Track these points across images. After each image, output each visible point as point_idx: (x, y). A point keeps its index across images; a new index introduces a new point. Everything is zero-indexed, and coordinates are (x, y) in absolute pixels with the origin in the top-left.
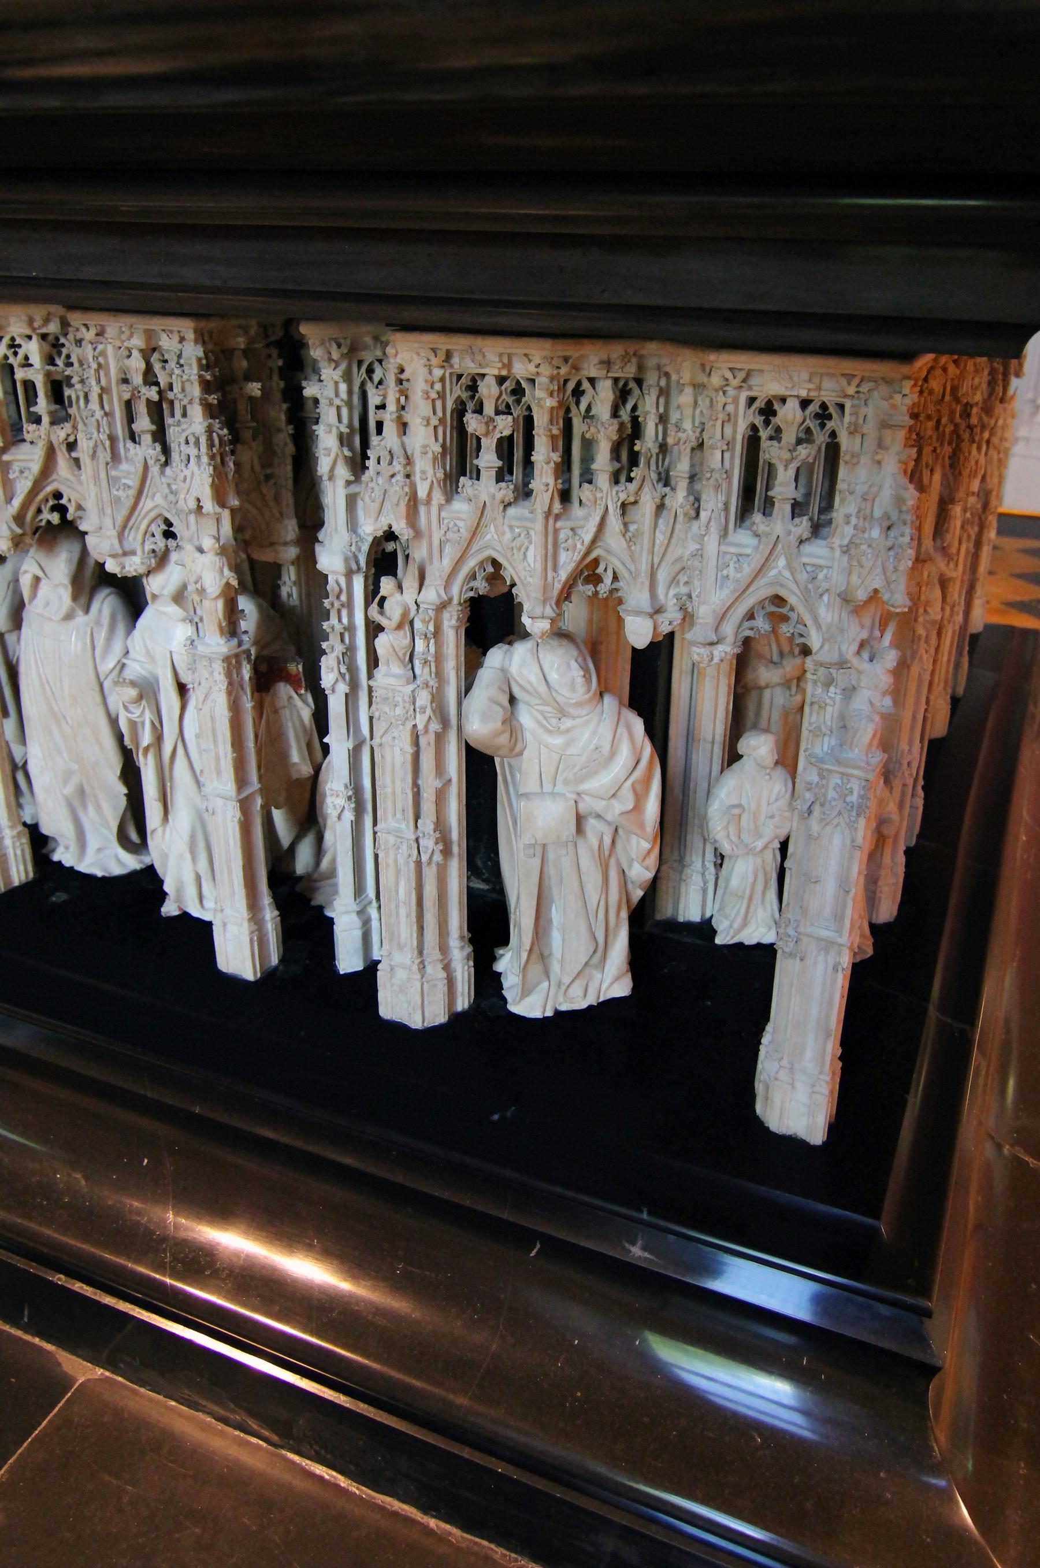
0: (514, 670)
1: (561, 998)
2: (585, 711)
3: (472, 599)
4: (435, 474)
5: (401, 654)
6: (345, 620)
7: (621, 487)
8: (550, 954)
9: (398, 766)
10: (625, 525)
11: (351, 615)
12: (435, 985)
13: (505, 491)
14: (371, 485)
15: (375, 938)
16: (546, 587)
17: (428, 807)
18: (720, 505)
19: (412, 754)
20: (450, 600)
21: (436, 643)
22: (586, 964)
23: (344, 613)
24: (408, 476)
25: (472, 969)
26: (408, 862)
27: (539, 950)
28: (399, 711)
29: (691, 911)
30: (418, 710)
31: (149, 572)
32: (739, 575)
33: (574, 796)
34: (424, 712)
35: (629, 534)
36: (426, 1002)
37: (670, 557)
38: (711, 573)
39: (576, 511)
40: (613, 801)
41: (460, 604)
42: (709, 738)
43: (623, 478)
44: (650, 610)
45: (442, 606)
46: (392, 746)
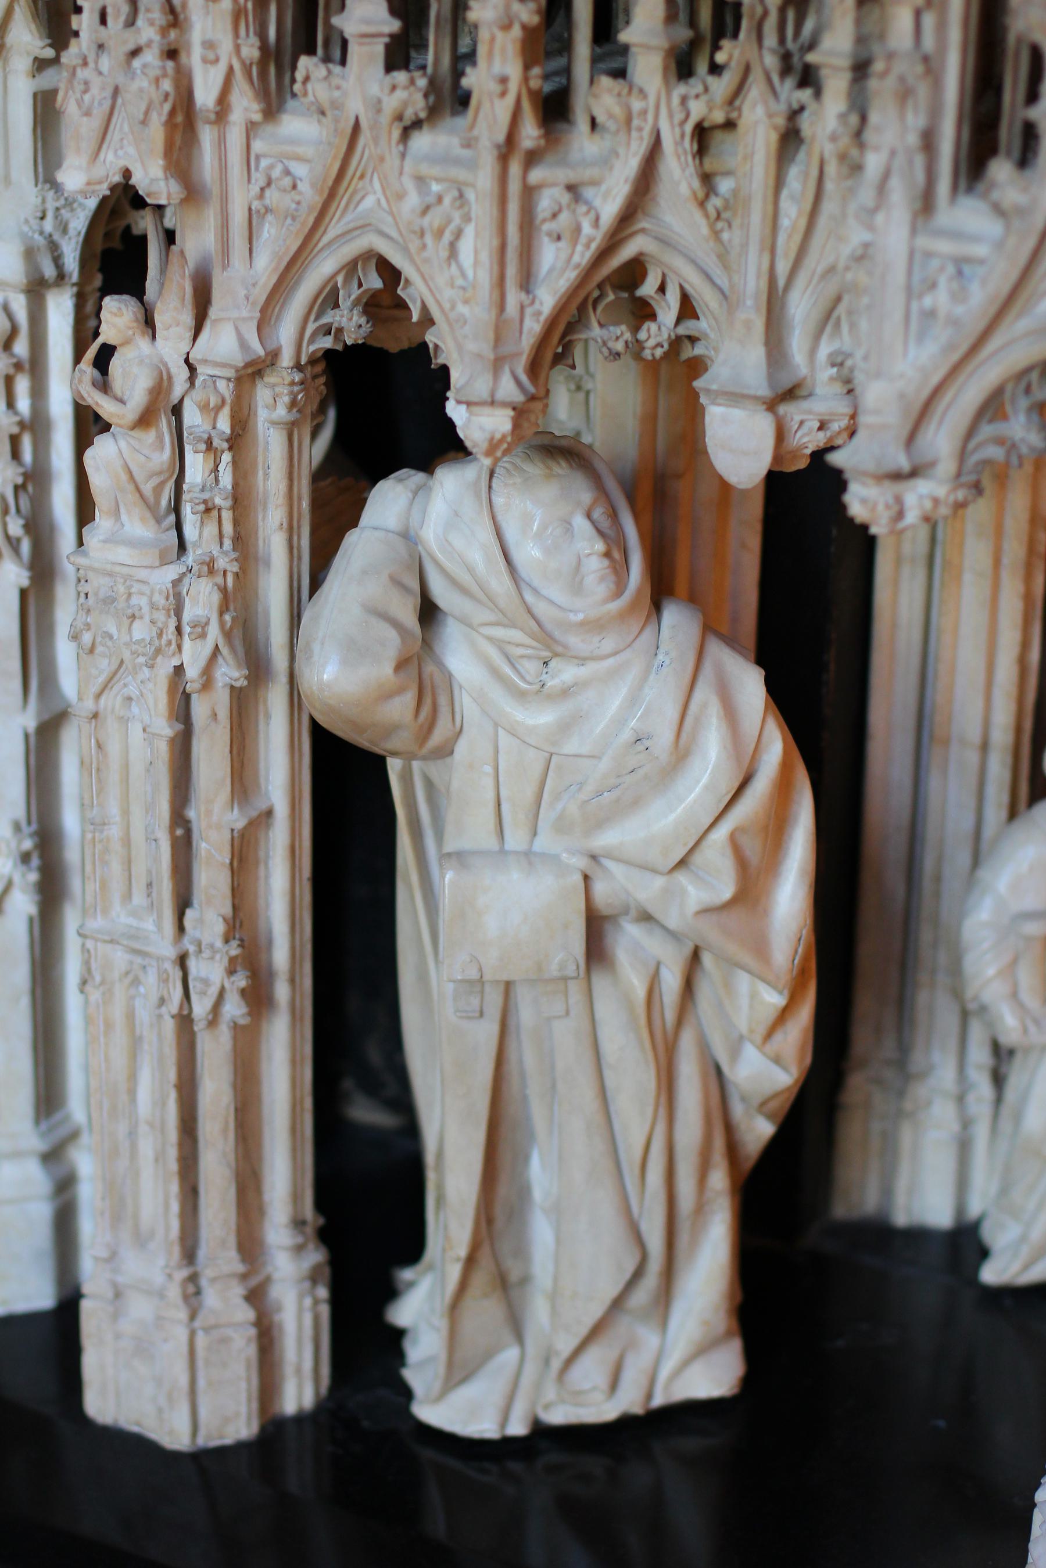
0: (431, 534)
1: (550, 1393)
2: (609, 644)
3: (329, 354)
4: (237, 48)
5: (147, 489)
6: (24, 404)
7: (694, 86)
8: (525, 1280)
9: (137, 769)
10: (707, 179)
11: (39, 392)
12: (225, 1341)
13: (407, 92)
14: (81, 74)
15: (89, 1228)
16: (499, 334)
17: (211, 878)
18: (913, 139)
19: (172, 741)
20: (274, 356)
21: (235, 463)
22: (617, 1304)
23: (22, 385)
24: (172, 54)
25: (325, 1310)
26: (160, 1016)
27: (496, 1257)
28: (140, 631)
29: (926, 1199)
30: (187, 630)
31: (456, 514)
32: (959, 310)
33: (580, 862)
34: (203, 636)
35: (715, 202)
36: (201, 1383)
37: (815, 262)
38: (895, 301)
39: (582, 143)
40: (682, 878)
41: (298, 367)
42: (974, 734)
43: (702, 67)
44: (764, 391)
45: (252, 372)
46: (124, 721)
